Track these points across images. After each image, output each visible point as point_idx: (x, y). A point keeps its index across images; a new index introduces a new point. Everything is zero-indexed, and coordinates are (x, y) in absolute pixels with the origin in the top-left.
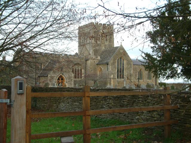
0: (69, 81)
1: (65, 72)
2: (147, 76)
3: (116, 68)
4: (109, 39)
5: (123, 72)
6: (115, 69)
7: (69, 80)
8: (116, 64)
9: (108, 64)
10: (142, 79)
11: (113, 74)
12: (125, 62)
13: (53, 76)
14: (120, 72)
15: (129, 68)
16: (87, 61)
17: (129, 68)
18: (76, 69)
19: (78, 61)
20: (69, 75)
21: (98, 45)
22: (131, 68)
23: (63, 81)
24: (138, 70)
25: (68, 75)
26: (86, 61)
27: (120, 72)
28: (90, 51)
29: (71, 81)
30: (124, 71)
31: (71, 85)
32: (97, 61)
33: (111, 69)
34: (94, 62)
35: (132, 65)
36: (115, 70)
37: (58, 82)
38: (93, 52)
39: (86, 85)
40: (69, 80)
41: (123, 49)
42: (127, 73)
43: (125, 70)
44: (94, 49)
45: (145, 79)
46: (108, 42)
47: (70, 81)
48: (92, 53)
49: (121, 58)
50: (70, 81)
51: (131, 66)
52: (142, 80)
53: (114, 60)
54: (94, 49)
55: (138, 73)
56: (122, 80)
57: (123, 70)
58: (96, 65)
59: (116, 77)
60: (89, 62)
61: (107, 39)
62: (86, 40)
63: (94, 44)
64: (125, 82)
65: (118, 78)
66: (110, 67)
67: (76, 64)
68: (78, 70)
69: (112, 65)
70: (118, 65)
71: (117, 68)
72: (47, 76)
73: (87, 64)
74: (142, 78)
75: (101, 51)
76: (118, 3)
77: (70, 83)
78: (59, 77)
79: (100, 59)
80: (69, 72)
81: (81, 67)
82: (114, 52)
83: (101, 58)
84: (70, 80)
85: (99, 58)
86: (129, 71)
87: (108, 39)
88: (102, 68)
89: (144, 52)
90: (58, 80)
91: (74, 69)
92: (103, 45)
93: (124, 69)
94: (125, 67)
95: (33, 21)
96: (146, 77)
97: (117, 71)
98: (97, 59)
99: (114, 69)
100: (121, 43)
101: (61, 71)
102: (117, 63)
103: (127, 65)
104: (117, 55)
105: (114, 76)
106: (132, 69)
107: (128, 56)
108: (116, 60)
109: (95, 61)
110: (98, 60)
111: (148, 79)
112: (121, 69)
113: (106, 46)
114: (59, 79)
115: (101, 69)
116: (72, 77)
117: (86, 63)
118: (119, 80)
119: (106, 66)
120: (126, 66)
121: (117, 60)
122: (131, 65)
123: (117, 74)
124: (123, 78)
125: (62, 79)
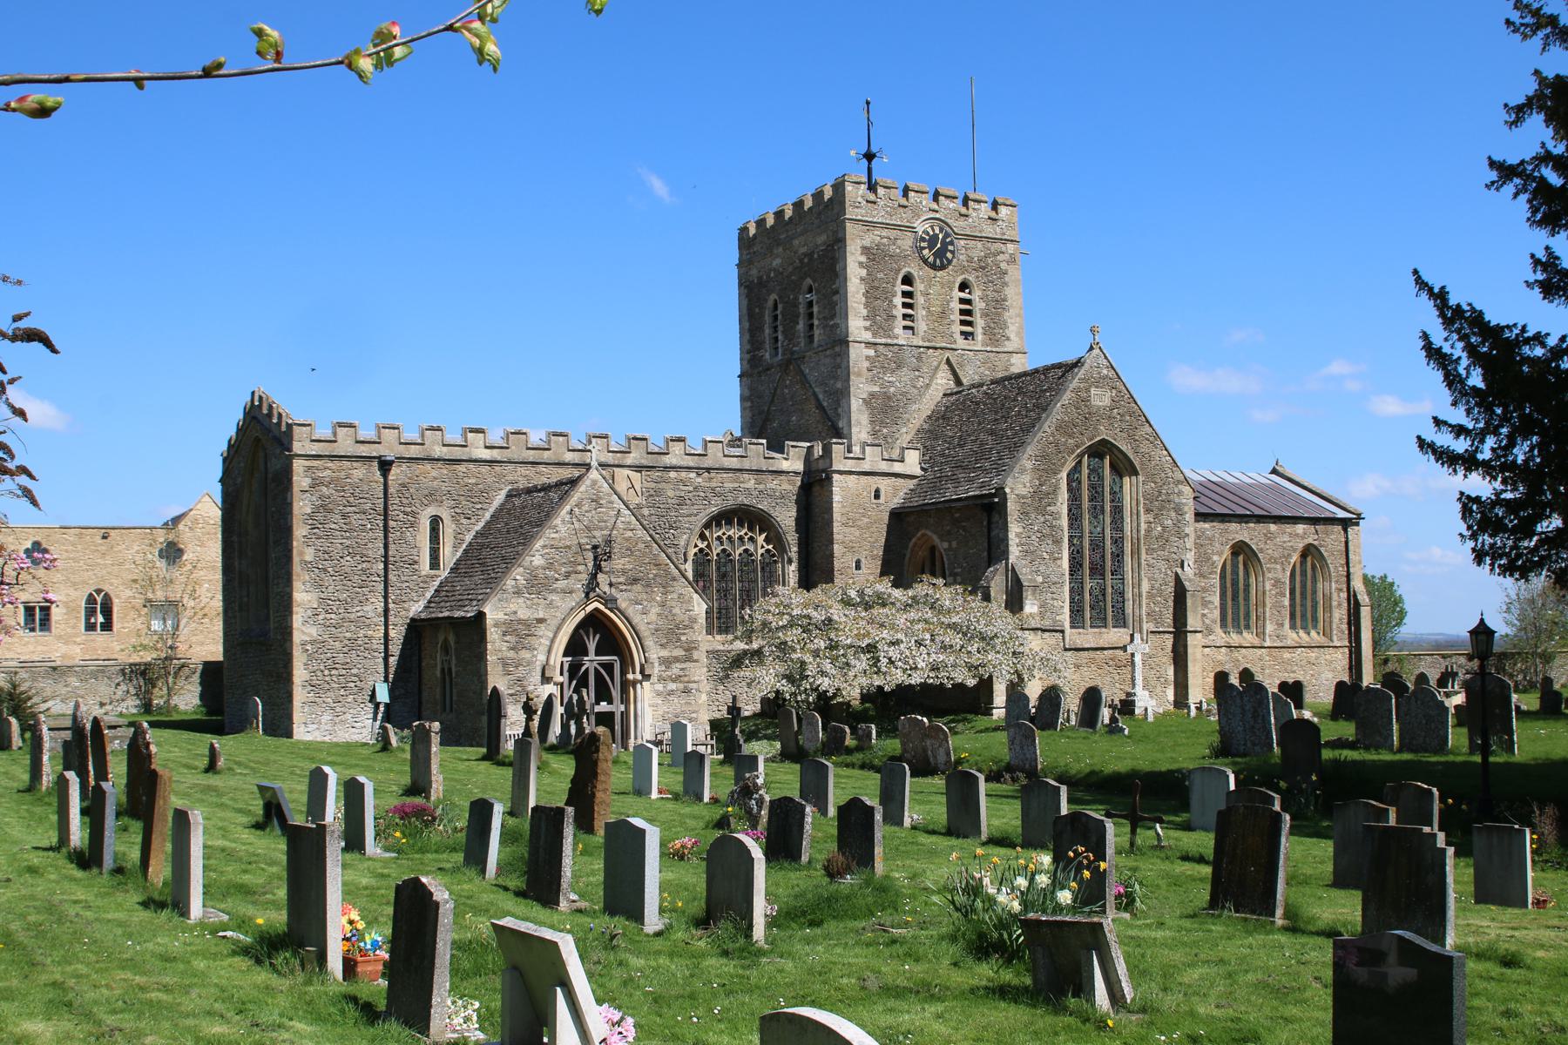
0: (667, 662)
2: (1287, 602)
3: (1058, 542)
4: (985, 315)
5: (1118, 570)
6: (1051, 547)
7: (665, 653)
8: (1062, 505)
12: (1476, 380)
13: (526, 623)
20: (663, 605)
22: (1182, 536)
24: (1215, 558)
29: (689, 659)
31: (687, 691)
32: (896, 489)
34: (877, 496)
44: (872, 395)
45: (1269, 628)
47: (677, 659)
50: (677, 659)
52: (1245, 634)
53: (1046, 469)
55: (1216, 580)
56: (1115, 635)
57: (1118, 557)
59: (1065, 617)
62: (801, 326)
63: (871, 352)
70: (1074, 518)
76: (868, 103)
84: (679, 652)
89: (1445, 423)
96: (1278, 606)
97: (1065, 563)
99: (1048, 546)
102: (1063, 495)
106: (1190, 543)
109: (884, 484)
112: (1097, 545)
114: (575, 648)
116: (693, 620)
123: (1067, 588)
125: (612, 642)
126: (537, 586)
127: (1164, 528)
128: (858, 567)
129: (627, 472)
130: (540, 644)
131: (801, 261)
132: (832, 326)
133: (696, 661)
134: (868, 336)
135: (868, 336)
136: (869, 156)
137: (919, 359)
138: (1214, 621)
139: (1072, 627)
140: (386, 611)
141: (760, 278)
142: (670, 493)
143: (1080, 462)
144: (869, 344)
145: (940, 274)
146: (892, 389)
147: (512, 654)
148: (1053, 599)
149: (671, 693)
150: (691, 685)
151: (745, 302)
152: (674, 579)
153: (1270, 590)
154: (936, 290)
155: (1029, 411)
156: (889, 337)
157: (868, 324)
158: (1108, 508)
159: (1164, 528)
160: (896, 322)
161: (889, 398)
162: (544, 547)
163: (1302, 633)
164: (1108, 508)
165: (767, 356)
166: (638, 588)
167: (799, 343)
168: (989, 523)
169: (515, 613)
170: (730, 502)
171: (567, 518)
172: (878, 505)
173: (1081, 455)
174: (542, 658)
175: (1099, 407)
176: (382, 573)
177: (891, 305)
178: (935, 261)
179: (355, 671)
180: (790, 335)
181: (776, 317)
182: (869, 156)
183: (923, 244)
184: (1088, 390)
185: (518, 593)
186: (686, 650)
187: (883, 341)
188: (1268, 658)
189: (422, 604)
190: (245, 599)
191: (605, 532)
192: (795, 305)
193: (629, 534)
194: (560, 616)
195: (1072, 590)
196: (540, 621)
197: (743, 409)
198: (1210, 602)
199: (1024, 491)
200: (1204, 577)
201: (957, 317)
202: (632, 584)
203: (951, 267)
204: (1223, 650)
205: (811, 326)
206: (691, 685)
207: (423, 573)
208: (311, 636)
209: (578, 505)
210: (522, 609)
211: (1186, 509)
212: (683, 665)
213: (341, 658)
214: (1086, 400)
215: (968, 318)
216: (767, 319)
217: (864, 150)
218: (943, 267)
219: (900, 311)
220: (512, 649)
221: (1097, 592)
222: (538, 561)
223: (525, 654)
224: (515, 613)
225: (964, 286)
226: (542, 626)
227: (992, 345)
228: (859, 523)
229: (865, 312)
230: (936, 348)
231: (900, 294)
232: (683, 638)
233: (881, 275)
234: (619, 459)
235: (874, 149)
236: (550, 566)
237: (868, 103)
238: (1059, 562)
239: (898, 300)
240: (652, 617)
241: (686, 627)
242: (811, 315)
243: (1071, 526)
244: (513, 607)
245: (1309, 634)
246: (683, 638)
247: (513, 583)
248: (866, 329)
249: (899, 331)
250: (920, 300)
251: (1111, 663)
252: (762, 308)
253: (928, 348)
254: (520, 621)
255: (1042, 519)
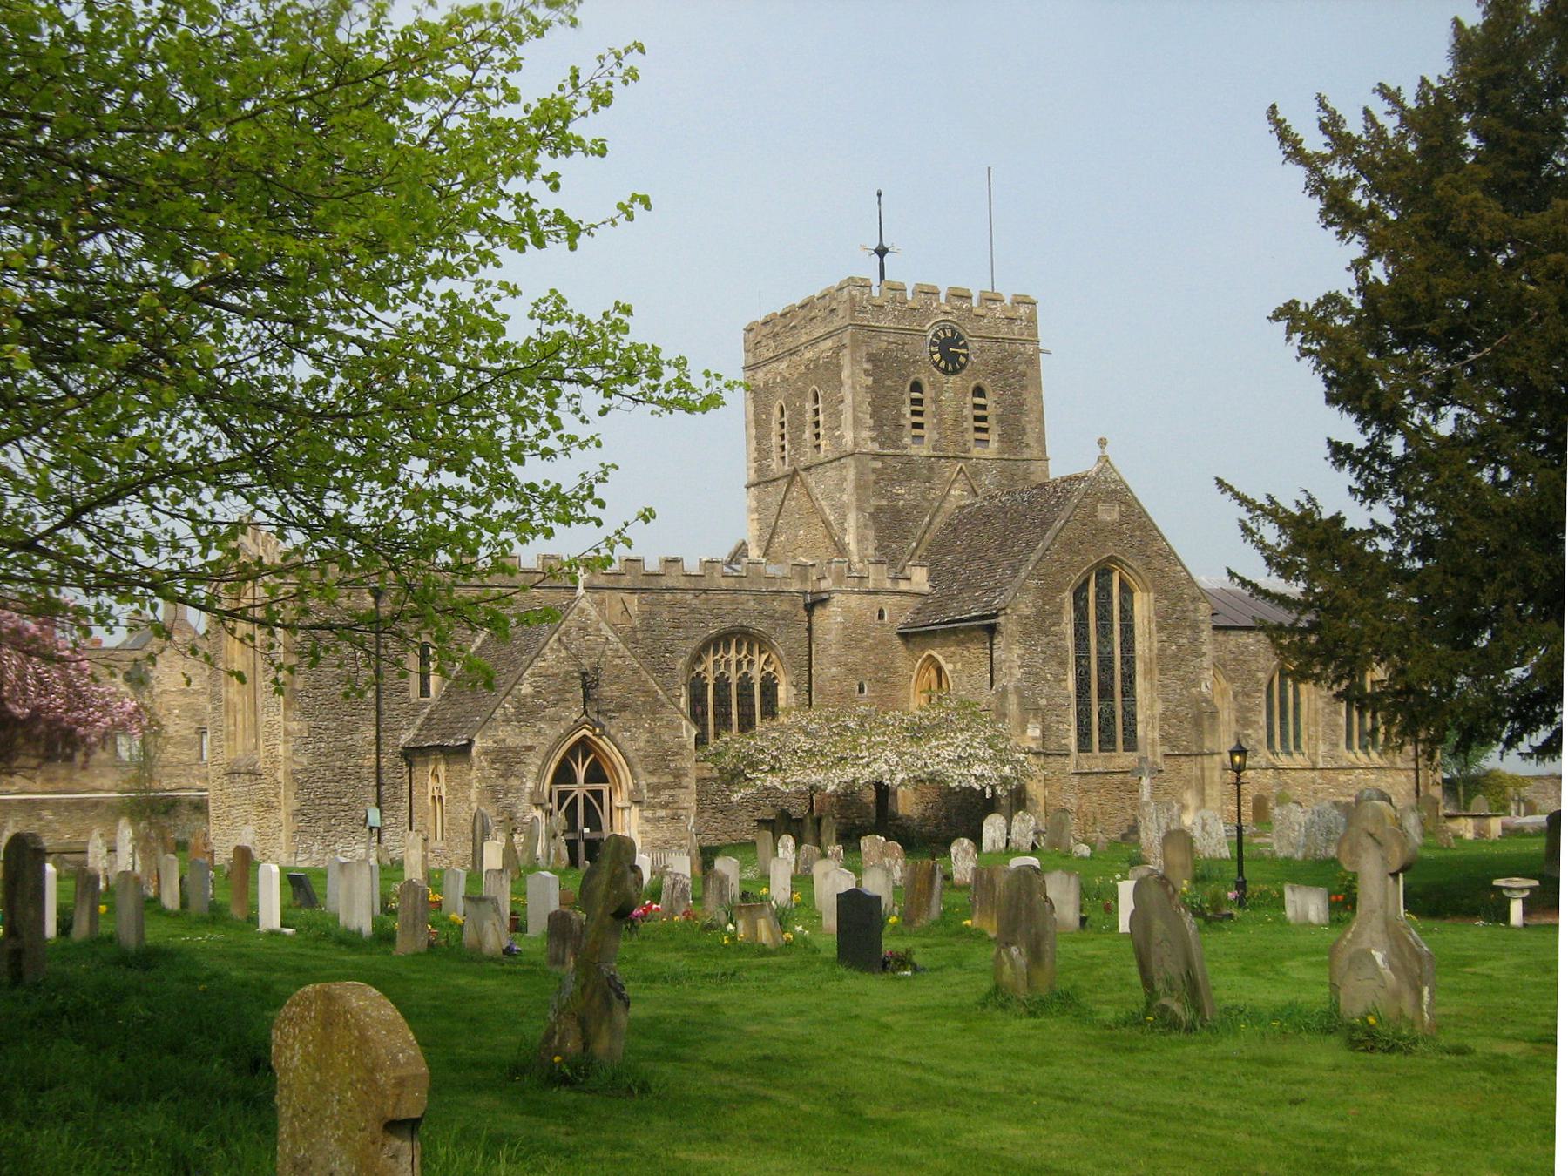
0: (655, 789)
1: (623, 707)
3: (1063, 664)
4: (1001, 421)
5: (1129, 691)
6: (1055, 669)
7: (654, 780)
9: (992, 630)
10: (1297, 747)
11: (1037, 710)
12: (1143, 606)
13: (515, 751)
14: (1106, 692)
15: (1179, 659)
16: (818, 611)
17: (1179, 659)
18: (722, 684)
19: (746, 612)
21: (908, 469)
23: (605, 788)
25: (643, 737)
26: (810, 608)
27: (1101, 697)
28: (842, 520)
29: (678, 786)
30: (1139, 679)
31: (674, 818)
32: (902, 609)
33: (1018, 673)
34: (881, 616)
35: (1206, 634)
36: (1060, 680)
37: (563, 796)
38: (871, 534)
39: (87, 41)
40: (654, 780)
41: (1121, 496)
42: (1165, 700)
43: (1148, 672)
44: (879, 509)
46: (994, 444)
47: (667, 786)
48: (861, 540)
49: (1104, 572)
50: (667, 786)
51: (1194, 641)
53: (1048, 592)
54: (874, 502)
55: (1262, 699)
56: (1123, 759)
57: (1129, 678)
58: (898, 642)
59: (1072, 741)
60: (831, 620)
61: (984, 419)
62: (808, 435)
63: (878, 464)
64: (1145, 781)
65: (1084, 744)
66: (1009, 652)
67: (721, 640)
68: (722, 684)
69: (1026, 634)
71: (1078, 659)
72: (465, 749)
73: (817, 632)
74: (1297, 736)
75: (940, 521)
76: (879, 195)
77: (665, 806)
78: (572, 752)
79: (926, 588)
80: (655, 707)
81: (767, 662)
82: (1046, 524)
83: (932, 577)
85: (920, 579)
86: (1178, 686)
87: (992, 423)
88: (948, 667)
90: (555, 781)
91: (710, 681)
92: (950, 470)
93: (1139, 667)
94: (1141, 646)
95: (378, 732)
98: (903, 586)
100: (1102, 443)
101: (586, 697)
102: (1069, 615)
103: (1161, 629)
104: (1068, 546)
105: (1046, 729)
107: (1169, 555)
108: (1063, 591)
109: (889, 604)
110: (907, 600)
111: (1349, 746)
113: (976, 474)
114: (564, 773)
115: (939, 670)
116: (683, 746)
117: (809, 630)
118: (1096, 760)
119: (977, 651)
120: (1155, 637)
121: (1068, 596)
122: (1195, 628)
124: (1131, 744)
125: (597, 774)
126: (527, 713)
127: (1180, 647)
128: (861, 690)
129: (622, 594)
130: (529, 771)
131: (807, 367)
132: (838, 437)
133: (686, 788)
134: (875, 447)
135: (875, 447)
136: (881, 252)
137: (930, 469)
138: (1259, 742)
139: (1079, 751)
140: (378, 738)
141: (766, 383)
142: (665, 615)
143: (1087, 582)
144: (876, 456)
145: (952, 378)
146: (901, 502)
147: (501, 781)
148: (1058, 722)
149: (660, 820)
150: (680, 812)
151: (751, 408)
152: (663, 706)
153: (1323, 709)
154: (950, 393)
155: (1036, 527)
156: (898, 447)
157: (874, 435)
158: (1117, 627)
159: (1180, 647)
160: (905, 433)
161: (899, 511)
162: (533, 675)
163: (1360, 754)
164: (1117, 627)
165: (774, 465)
166: (628, 715)
167: (806, 453)
168: (992, 644)
169: (504, 740)
170: (727, 623)
171: (556, 646)
172: (883, 625)
173: (1090, 570)
174: (530, 784)
175: (1107, 524)
176: (374, 700)
177: (901, 415)
178: (947, 365)
179: (344, 801)
180: (797, 442)
181: (782, 424)
182: (881, 252)
183: (933, 349)
184: (1095, 507)
185: (507, 721)
186: (675, 777)
187: (891, 451)
188: (1320, 781)
189: (413, 732)
190: (233, 728)
191: (592, 660)
192: (801, 413)
193: (618, 661)
194: (549, 744)
195: (1079, 713)
196: (530, 748)
197: (256, 895)
198: (1255, 722)
199: (1026, 612)
200: (1248, 696)
201: (970, 424)
202: (620, 711)
203: (964, 372)
204: (1270, 772)
205: (817, 436)
206: (680, 812)
207: (414, 701)
208: (300, 764)
209: (567, 633)
210: (510, 736)
211: (1203, 626)
212: (672, 792)
213: (331, 787)
214: (1093, 516)
215: (983, 425)
216: (775, 427)
217: (876, 245)
218: (955, 372)
219: (908, 419)
220: (502, 776)
221: (1105, 715)
222: (526, 689)
223: (514, 782)
224: (504, 740)
225: (979, 391)
226: (532, 753)
227: (1010, 452)
228: (864, 644)
229: (870, 422)
230: (948, 458)
231: (908, 402)
232: (672, 765)
233: (888, 383)
234: (612, 582)
235: (886, 245)
236: (538, 693)
237: (879, 195)
238: (1063, 684)
239: (907, 410)
240: (641, 743)
241: (677, 753)
242: (817, 424)
243: (1077, 646)
244: (501, 735)
245: (1368, 754)
246: (672, 765)
247: (502, 711)
248: (873, 440)
249: (907, 441)
250: (928, 407)
251: (1122, 788)
252: (769, 415)
253: (940, 458)
254: (509, 749)
255: (1046, 640)
